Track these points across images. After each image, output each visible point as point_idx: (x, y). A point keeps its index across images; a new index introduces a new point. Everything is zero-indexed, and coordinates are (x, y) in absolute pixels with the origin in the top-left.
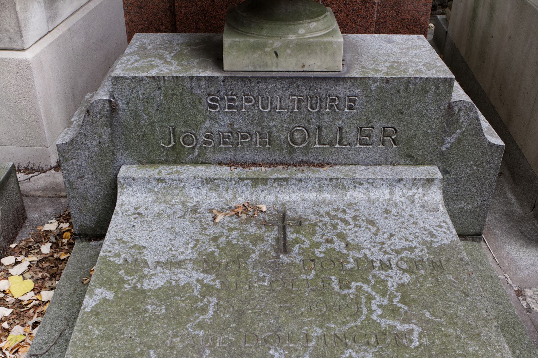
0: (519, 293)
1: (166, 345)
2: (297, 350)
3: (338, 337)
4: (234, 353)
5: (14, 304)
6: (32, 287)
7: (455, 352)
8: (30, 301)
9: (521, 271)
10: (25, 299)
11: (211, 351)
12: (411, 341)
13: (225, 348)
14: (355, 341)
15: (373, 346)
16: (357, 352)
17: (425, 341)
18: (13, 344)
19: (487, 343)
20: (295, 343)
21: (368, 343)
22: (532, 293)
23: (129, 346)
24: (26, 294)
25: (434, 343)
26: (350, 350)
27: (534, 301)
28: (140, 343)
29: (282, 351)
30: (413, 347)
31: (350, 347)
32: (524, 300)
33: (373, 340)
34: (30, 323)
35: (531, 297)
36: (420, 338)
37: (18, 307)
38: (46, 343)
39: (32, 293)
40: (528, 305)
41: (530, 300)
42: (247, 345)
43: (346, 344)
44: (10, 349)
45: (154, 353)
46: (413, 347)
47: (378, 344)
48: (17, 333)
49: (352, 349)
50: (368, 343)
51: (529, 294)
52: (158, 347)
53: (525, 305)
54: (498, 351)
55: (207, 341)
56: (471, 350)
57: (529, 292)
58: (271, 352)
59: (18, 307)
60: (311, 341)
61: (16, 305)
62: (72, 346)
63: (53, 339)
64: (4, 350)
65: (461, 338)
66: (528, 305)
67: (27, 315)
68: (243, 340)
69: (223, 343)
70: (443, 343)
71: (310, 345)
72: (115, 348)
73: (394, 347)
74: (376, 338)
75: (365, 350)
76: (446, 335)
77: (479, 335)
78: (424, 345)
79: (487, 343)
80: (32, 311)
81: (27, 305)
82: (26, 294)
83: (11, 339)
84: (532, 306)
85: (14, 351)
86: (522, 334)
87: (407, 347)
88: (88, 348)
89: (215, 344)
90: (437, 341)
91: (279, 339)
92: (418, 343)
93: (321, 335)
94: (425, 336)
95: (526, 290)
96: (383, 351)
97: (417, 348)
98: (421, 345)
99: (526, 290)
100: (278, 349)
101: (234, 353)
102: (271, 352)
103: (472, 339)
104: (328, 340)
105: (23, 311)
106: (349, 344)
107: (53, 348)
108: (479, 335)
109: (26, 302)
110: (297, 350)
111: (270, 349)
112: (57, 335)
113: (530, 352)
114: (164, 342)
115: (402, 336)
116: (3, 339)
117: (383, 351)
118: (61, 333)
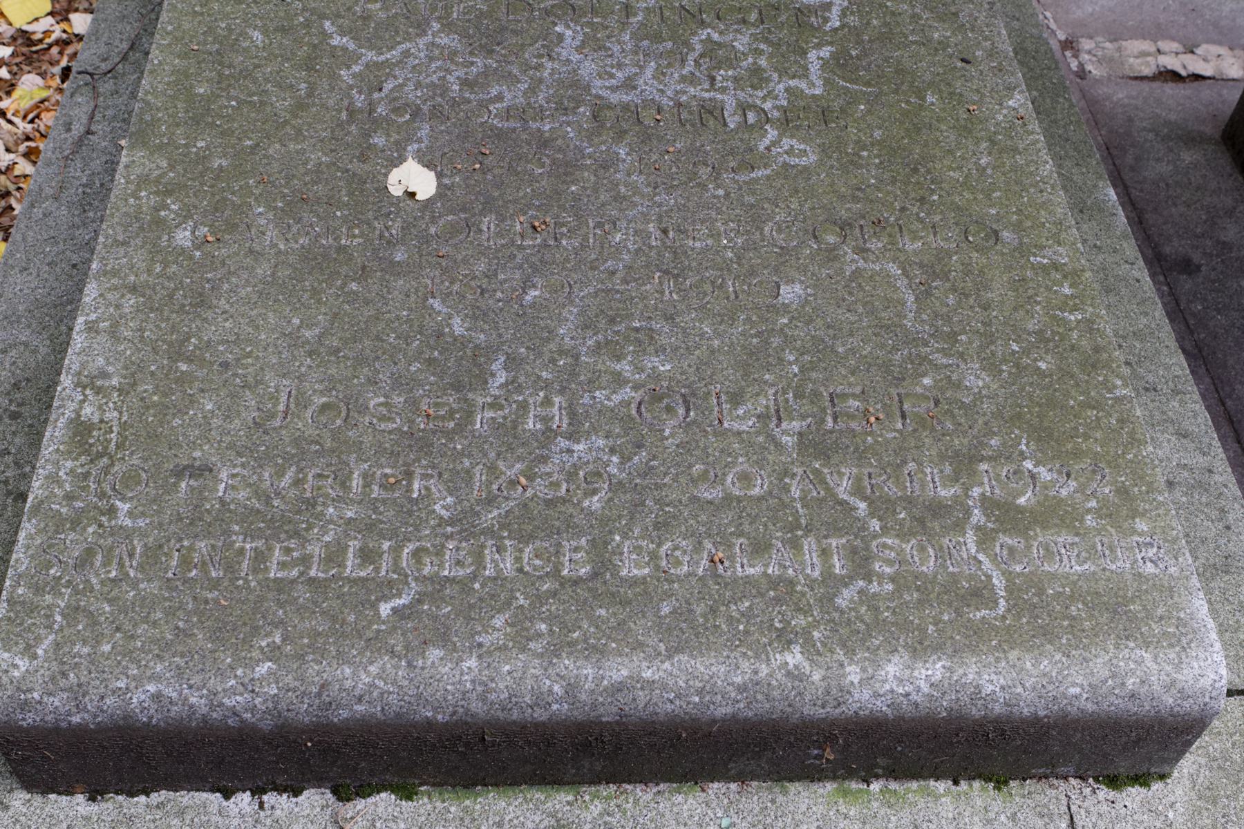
0: (1068, 44)
1: (354, 14)
2: (607, 27)
3: (688, 11)
4: (488, 29)
5: (14, 39)
6: (49, 8)
7: (906, 37)
8: (47, 33)
9: (1079, 7)
10: (38, 29)
11: (442, 24)
12: (826, 20)
13: (468, 21)
14: (719, 18)
15: (753, 25)
16: (721, 33)
17: (852, 20)
18: (25, 104)
19: (968, 26)
20: (605, 18)
21: (744, 21)
22: (1093, 45)
23: (282, 14)
24: (37, 19)
25: (868, 23)
26: (709, 30)
27: (1094, 59)
28: (303, 10)
29: (579, 28)
30: (827, 29)
31: (709, 26)
32: (1076, 56)
33: (753, 16)
34: (57, 70)
35: (1089, 52)
36: (843, 14)
37: (22, 44)
38: (105, 60)
39: (50, 20)
40: (1081, 65)
41: (1087, 57)
42: (511, 17)
43: (703, 22)
44: (22, 113)
45: (333, 24)
46: (827, 29)
47: (762, 22)
48: (30, 87)
49: (713, 28)
50: (744, 21)
51: (1087, 47)
52: (338, 16)
53: (1074, 65)
54: (986, 39)
55: (434, 9)
56: (936, 35)
57: (1086, 44)
58: (557, 29)
59: (22, 44)
60: (635, 15)
61: (20, 41)
62: (168, 11)
63: (119, 53)
64: (9, 116)
65: (921, 19)
66: (1081, 65)
67: (46, 58)
68: (505, 11)
69: (465, 14)
70: (886, 24)
71: (633, 20)
72: (255, 15)
73: (792, 27)
74: (760, 13)
75: (737, 31)
76: (893, 14)
77: (956, 14)
78: (849, 27)
79: (968, 26)
80: (55, 50)
81: (41, 41)
82: (37, 19)
83: (21, 98)
84: (1089, 67)
85: (30, 117)
86: (1049, 68)
87: (819, 28)
88: (202, 14)
89: (449, 15)
90: (875, 22)
91: (574, 10)
92: (838, 23)
93: (654, 7)
94: (852, 13)
95: (1082, 40)
96: (770, 32)
97: (835, 30)
98: (843, 26)
99: (1082, 40)
100: (572, 25)
101: (488, 29)
102: (557, 29)
103: (941, 19)
104: (667, 13)
105: (36, 52)
106: (708, 20)
107: (120, 66)
108: (956, 14)
109: (39, 36)
110: (607, 27)
111: (556, 25)
112: (125, 46)
113: (1058, 96)
114: (349, 9)
115: (810, 11)
116: (4, 96)
117: (770, 32)
118: (133, 44)
